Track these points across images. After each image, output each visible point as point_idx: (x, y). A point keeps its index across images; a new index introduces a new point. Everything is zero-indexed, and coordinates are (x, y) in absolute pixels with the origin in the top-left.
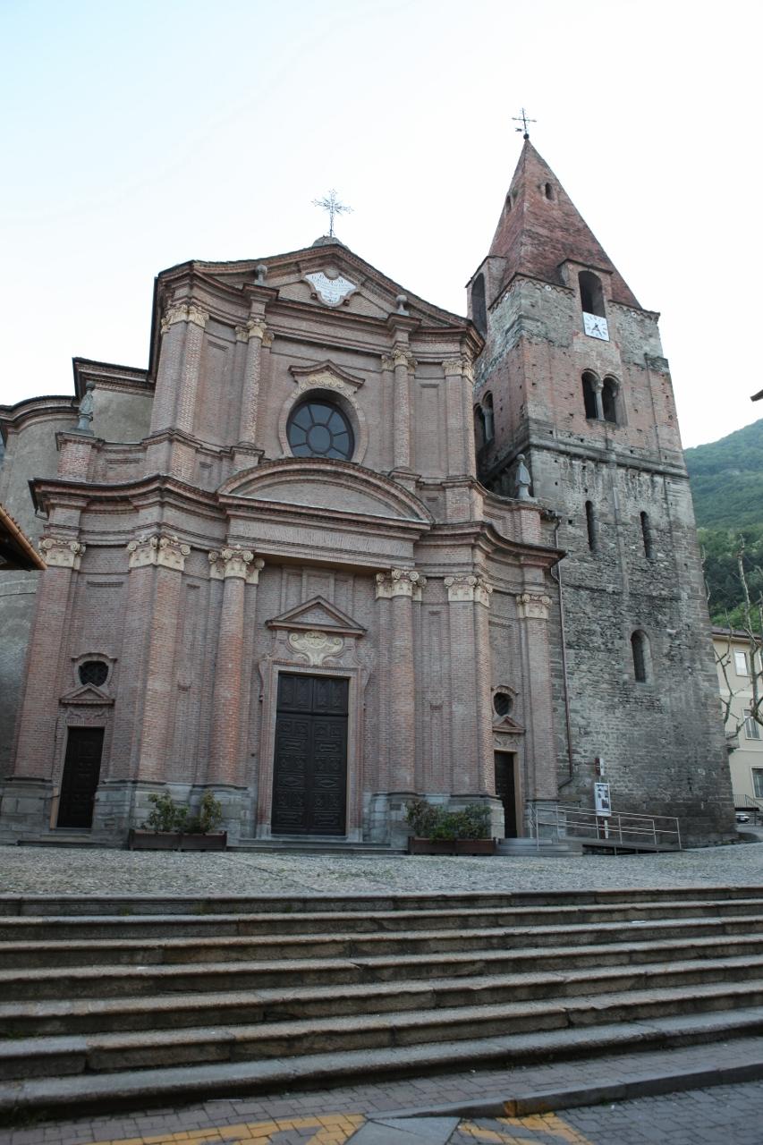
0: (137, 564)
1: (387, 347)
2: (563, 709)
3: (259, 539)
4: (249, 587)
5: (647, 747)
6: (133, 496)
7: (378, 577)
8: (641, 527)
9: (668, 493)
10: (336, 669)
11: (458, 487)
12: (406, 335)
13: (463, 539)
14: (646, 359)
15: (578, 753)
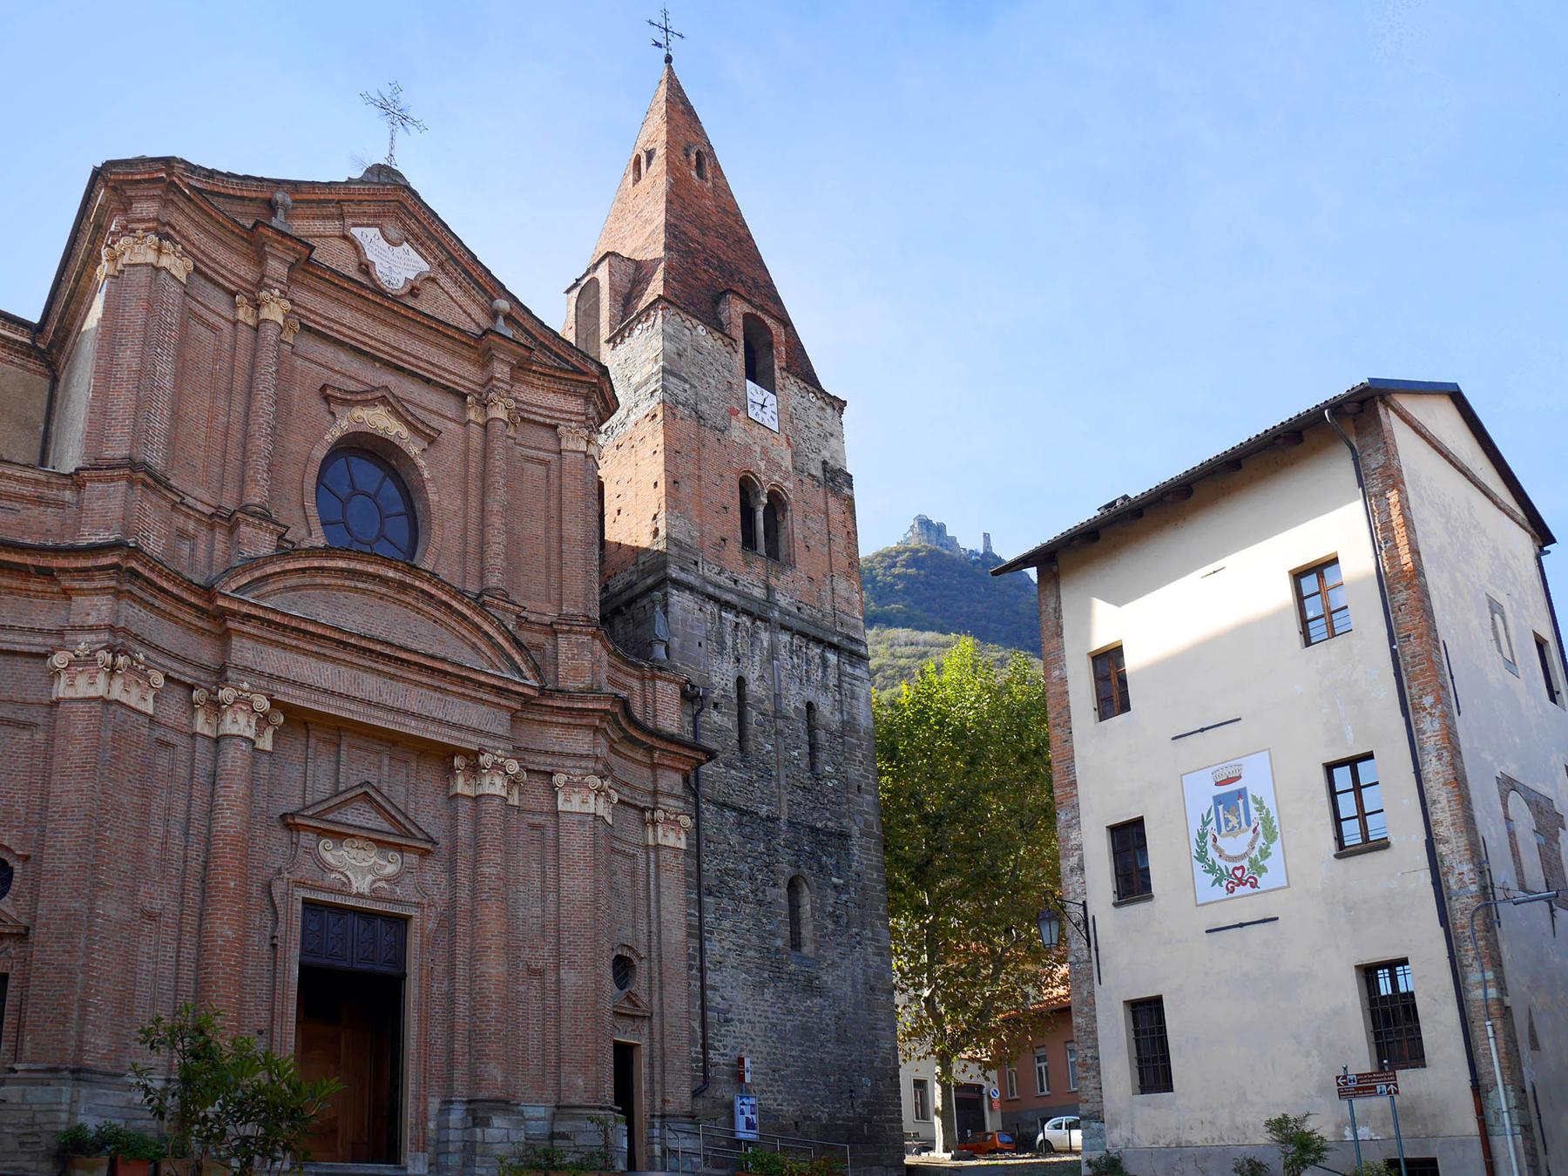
0: (70, 693)
4: (258, 755)
6: (63, 570)
7: (457, 762)
10: (390, 901)
14: (824, 470)
15: (716, 1049)
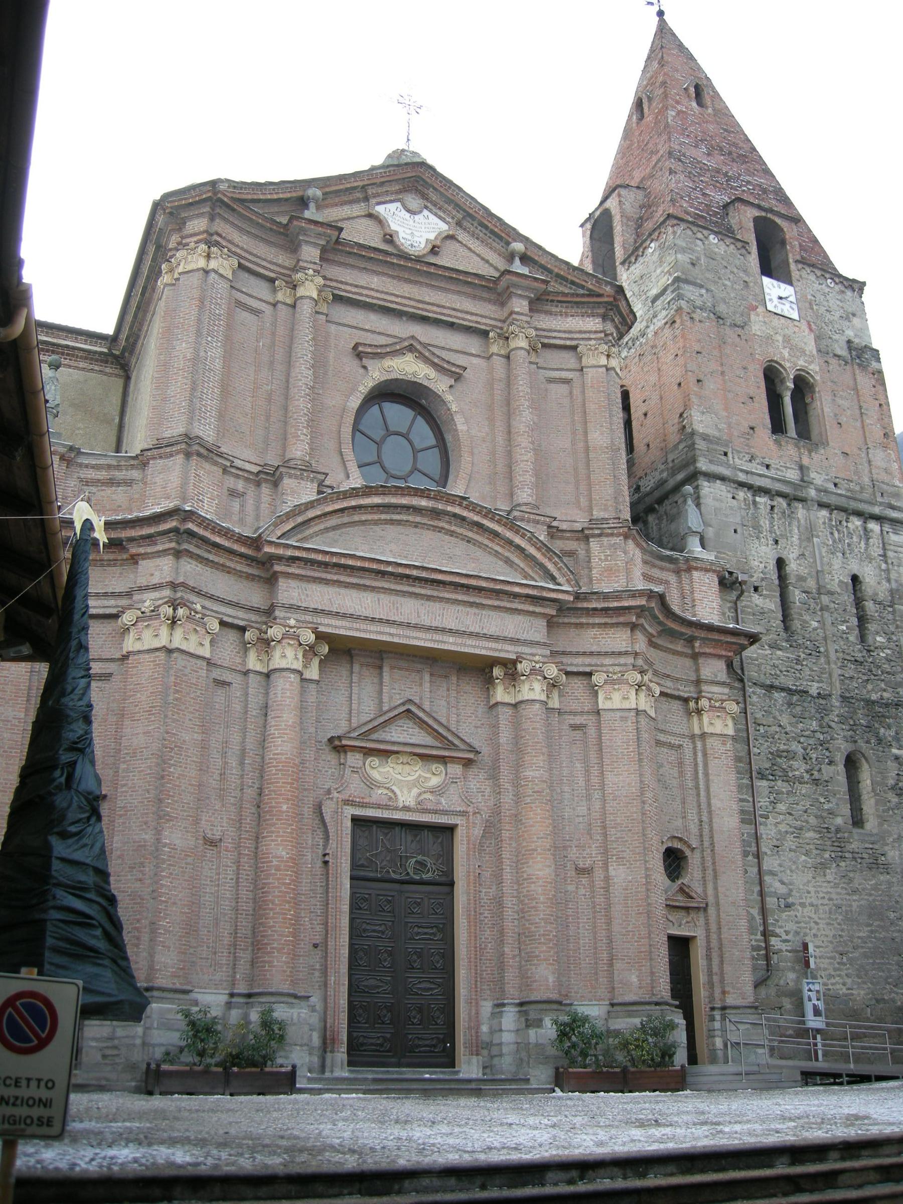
0: (138, 646)
1: (495, 319)
2: (756, 870)
3: (322, 611)
4: (305, 684)
5: (871, 925)
6: (131, 540)
7: (497, 672)
8: (853, 596)
9: (888, 547)
10: (435, 812)
11: (608, 535)
12: (525, 303)
13: (620, 615)
15: (777, 936)
